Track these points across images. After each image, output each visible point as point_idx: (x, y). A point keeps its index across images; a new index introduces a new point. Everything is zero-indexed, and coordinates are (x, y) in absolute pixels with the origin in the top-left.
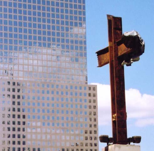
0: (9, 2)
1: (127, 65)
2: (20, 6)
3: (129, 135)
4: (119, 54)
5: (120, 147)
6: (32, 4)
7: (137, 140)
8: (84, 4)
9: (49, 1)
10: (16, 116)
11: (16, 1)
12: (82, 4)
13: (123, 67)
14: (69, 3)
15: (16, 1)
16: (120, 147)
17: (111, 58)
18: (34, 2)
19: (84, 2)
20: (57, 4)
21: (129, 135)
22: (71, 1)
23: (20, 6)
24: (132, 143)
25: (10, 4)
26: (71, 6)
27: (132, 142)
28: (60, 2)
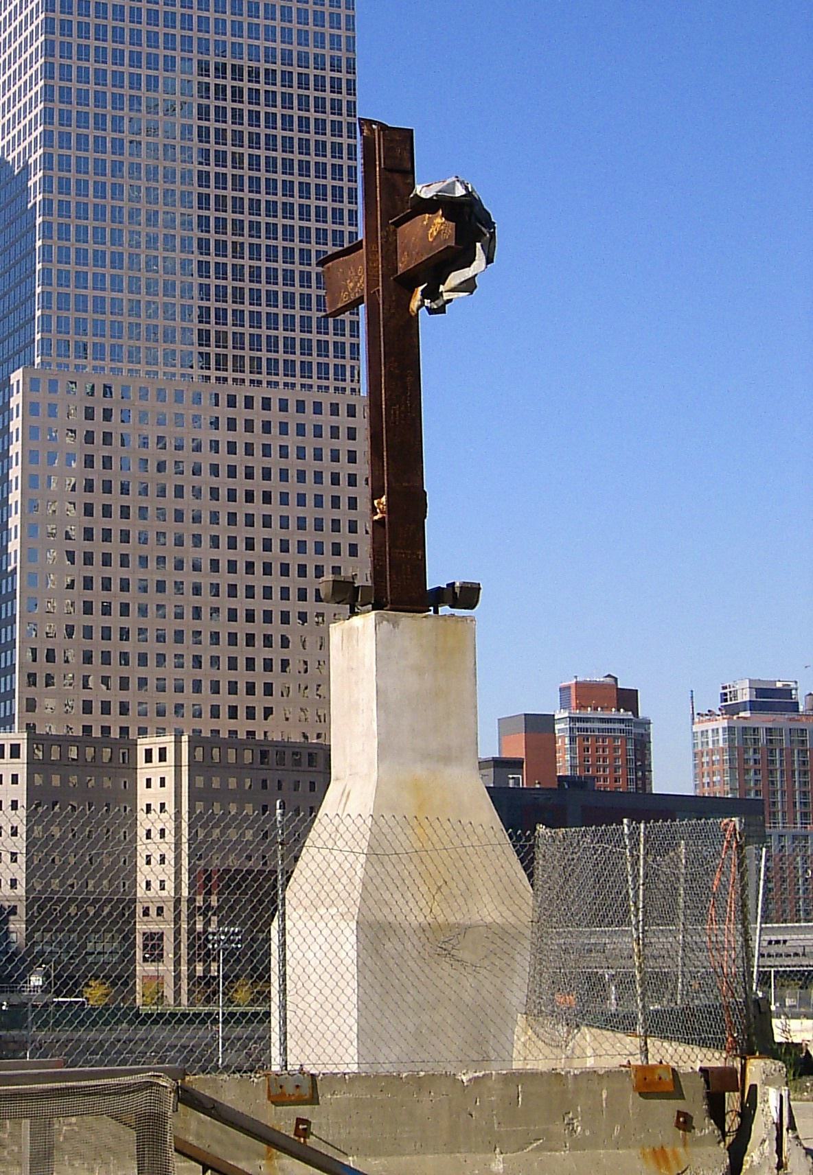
0: (283, 7)
1: (431, 311)
2: (170, 20)
3: (435, 579)
4: (401, 268)
5: (395, 624)
6: (212, 15)
7: (466, 596)
8: (350, 13)
9: (105, 5)
10: (343, 433)
11: (307, 3)
12: (343, 12)
13: (412, 322)
14: (327, 9)
15: (307, 3)
16: (395, 624)
17: (371, 282)
18: (220, 9)
19: (350, 5)
20: (153, 17)
21: (435, 579)
22: (203, 4)
23: (319, 19)
24: (444, 610)
25: (286, 14)
26: (186, 20)
27: (444, 603)
28: (144, 5)
